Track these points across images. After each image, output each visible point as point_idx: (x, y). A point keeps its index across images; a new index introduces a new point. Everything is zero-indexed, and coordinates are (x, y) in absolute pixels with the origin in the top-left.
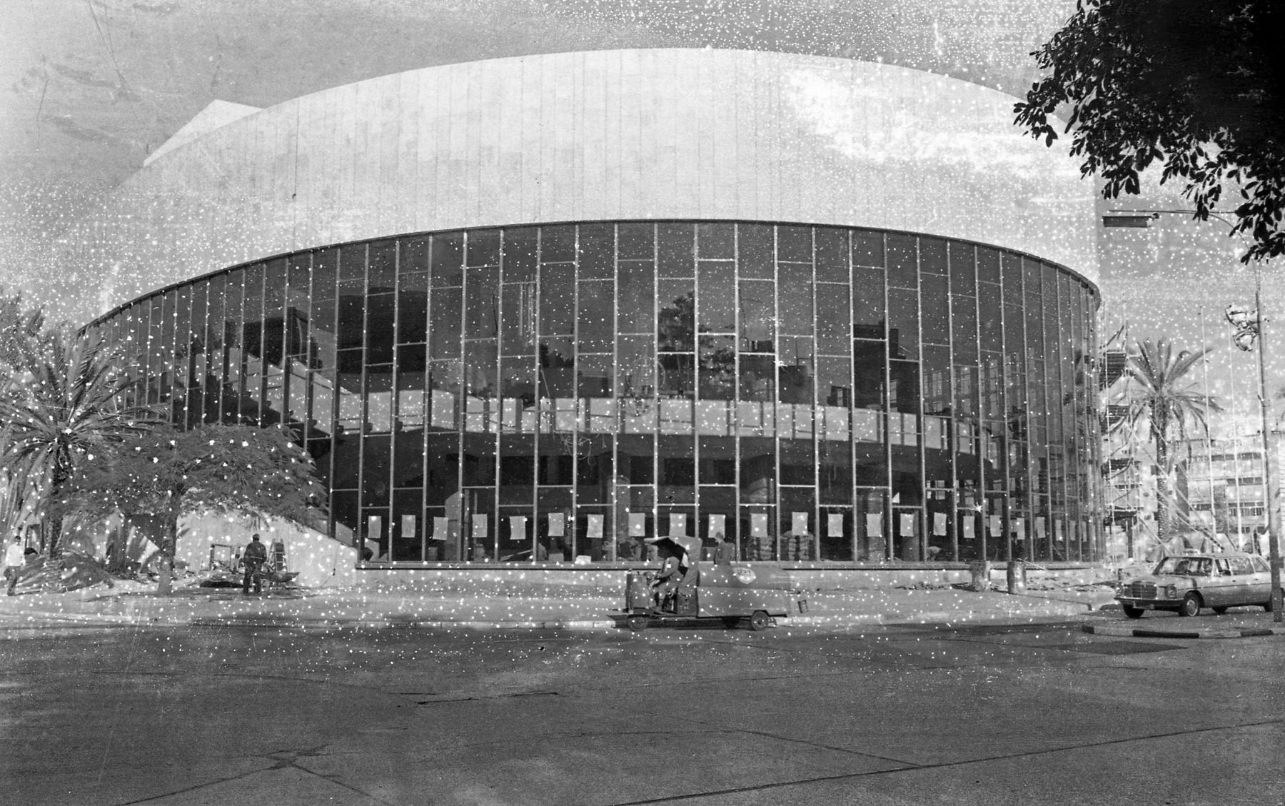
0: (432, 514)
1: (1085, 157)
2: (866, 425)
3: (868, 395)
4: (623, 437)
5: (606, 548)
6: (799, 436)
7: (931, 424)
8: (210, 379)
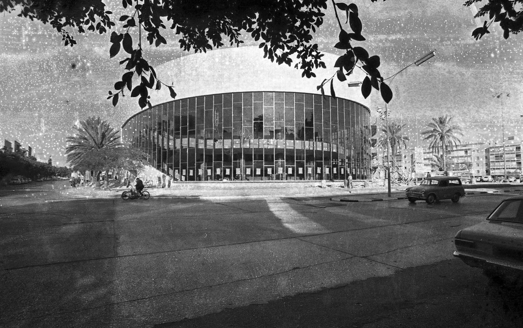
7: (325, 144)
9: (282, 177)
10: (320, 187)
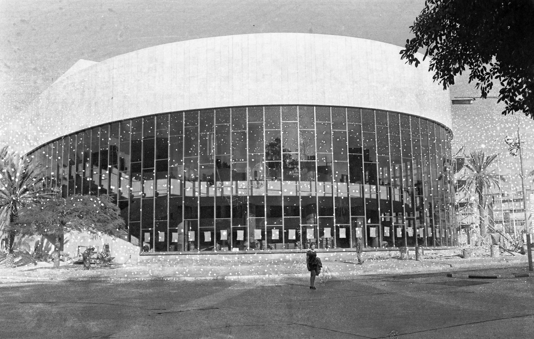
0: (171, 231)
1: (434, 72)
2: (355, 190)
3: (356, 178)
4: (252, 197)
5: (245, 244)
6: (327, 195)
8: (78, 176)
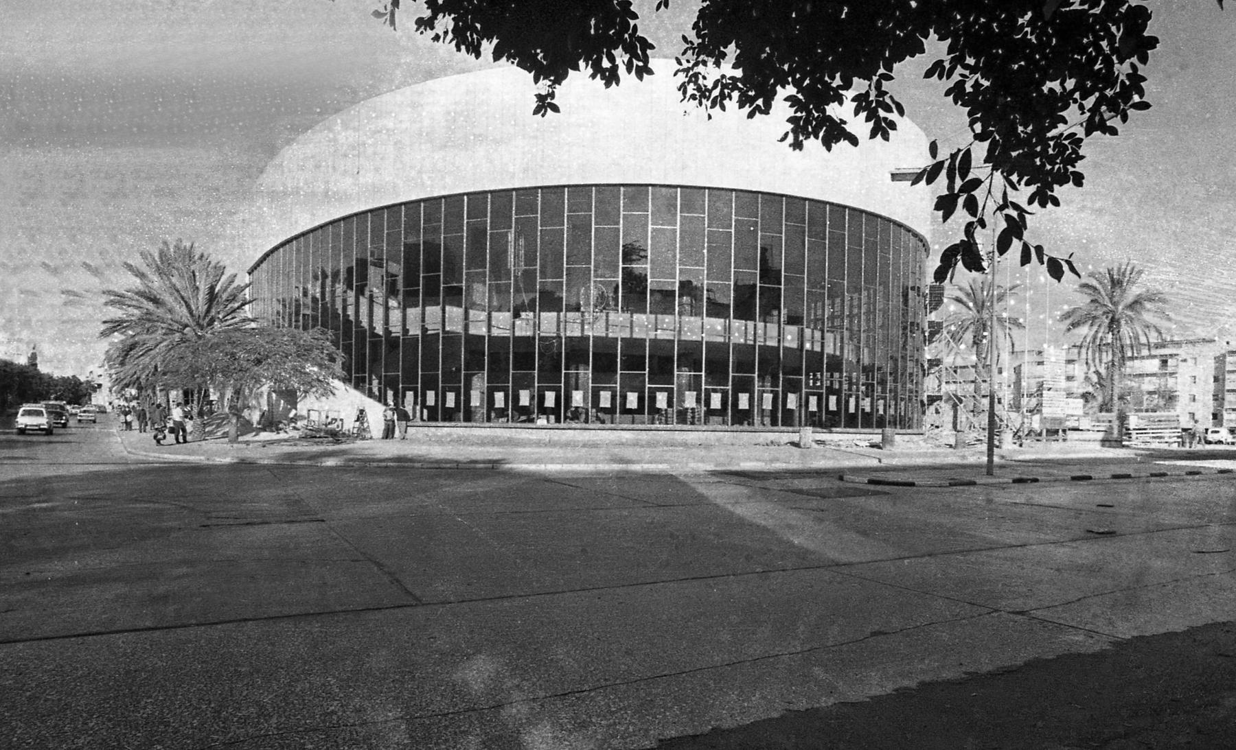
9: (693, 417)
10: (796, 445)
